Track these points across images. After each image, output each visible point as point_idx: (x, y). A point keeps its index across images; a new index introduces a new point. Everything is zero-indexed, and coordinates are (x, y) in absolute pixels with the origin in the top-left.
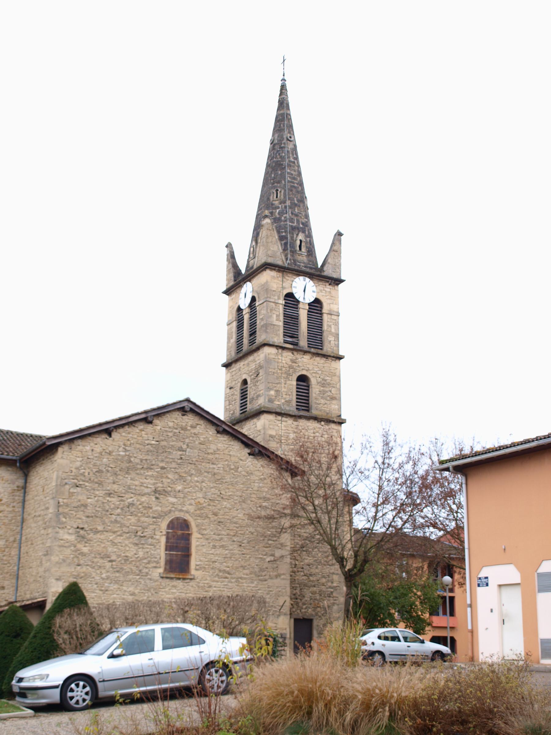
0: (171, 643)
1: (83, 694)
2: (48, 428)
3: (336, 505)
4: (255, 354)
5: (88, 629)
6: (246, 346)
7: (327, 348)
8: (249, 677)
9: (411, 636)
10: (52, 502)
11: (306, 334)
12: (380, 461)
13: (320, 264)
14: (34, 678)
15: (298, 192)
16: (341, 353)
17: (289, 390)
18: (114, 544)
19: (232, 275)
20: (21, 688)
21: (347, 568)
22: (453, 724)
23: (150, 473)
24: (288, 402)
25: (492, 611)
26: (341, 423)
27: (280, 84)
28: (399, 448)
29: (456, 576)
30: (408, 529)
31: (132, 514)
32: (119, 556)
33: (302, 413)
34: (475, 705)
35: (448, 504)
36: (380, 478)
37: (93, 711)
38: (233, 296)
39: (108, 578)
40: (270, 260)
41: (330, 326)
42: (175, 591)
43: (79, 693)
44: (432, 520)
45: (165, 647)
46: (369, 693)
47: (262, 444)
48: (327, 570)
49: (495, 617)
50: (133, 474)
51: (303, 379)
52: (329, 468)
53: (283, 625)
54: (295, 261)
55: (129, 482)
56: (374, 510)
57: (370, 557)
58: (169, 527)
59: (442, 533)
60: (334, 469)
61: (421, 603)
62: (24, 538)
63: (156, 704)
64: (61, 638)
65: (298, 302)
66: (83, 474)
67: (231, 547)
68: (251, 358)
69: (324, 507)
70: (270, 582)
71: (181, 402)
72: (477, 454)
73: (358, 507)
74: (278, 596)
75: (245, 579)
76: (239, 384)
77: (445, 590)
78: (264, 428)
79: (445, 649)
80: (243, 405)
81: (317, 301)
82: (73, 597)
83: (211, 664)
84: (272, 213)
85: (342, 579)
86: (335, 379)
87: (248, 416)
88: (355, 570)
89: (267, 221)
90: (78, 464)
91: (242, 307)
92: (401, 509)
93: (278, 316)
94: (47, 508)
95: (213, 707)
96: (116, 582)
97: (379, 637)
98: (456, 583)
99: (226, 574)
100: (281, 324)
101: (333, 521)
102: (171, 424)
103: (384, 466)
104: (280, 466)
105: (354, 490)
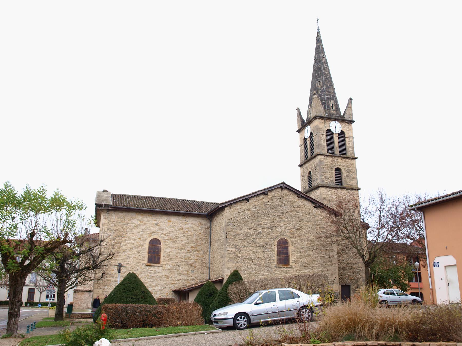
0: (284, 297)
1: (244, 322)
2: (219, 199)
3: (358, 229)
4: (314, 160)
5: (244, 291)
6: (309, 156)
7: (349, 154)
8: (323, 313)
9: (400, 292)
10: (223, 233)
11: (338, 148)
12: (379, 207)
13: (342, 115)
14: (221, 314)
15: (329, 81)
16: (356, 156)
17: (331, 177)
18: (253, 252)
19: (300, 123)
20: (215, 319)
21: (366, 260)
22: (428, 335)
23: (268, 218)
24: (332, 181)
25: (442, 279)
26: (358, 189)
27: (317, 31)
28: (388, 200)
29: (421, 262)
30: (395, 240)
31: (260, 237)
32: (256, 257)
33: (338, 186)
34: (439, 326)
35: (415, 227)
36: (380, 215)
37: (250, 329)
38: (302, 133)
39: (251, 268)
40: (318, 114)
41: (349, 144)
42: (282, 273)
43: (242, 321)
44: (406, 236)
45: (281, 300)
46: (384, 320)
47: (320, 202)
48: (356, 261)
49: (444, 282)
50: (260, 219)
51: (338, 170)
52: (354, 212)
53: (336, 288)
54: (330, 114)
55: (258, 223)
56: (377, 231)
57: (377, 254)
58: (278, 243)
59: (412, 241)
60: (356, 212)
61: (404, 276)
62: (211, 250)
63: (279, 326)
64: (232, 296)
65: (333, 133)
66: (237, 220)
67: (308, 252)
68: (312, 161)
69: (352, 230)
70: (328, 268)
71: (280, 184)
72: (428, 201)
73: (369, 230)
74: (332, 274)
75: (316, 266)
76: (307, 174)
77: (416, 270)
78: (321, 194)
79: (419, 299)
80: (310, 184)
81: (342, 132)
82: (236, 277)
83: (304, 307)
84: (317, 92)
85: (364, 265)
86: (354, 169)
87: (312, 189)
88: (370, 261)
89: (315, 96)
90: (234, 215)
91: (306, 138)
92: (391, 230)
93: (324, 140)
94: (222, 236)
95: (306, 327)
96: (255, 270)
97: (384, 293)
98: (421, 266)
99: (306, 264)
100: (326, 144)
101: (357, 237)
102: (276, 195)
103: (381, 209)
104: (329, 212)
105: (367, 222)
